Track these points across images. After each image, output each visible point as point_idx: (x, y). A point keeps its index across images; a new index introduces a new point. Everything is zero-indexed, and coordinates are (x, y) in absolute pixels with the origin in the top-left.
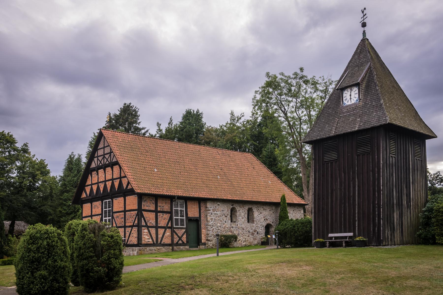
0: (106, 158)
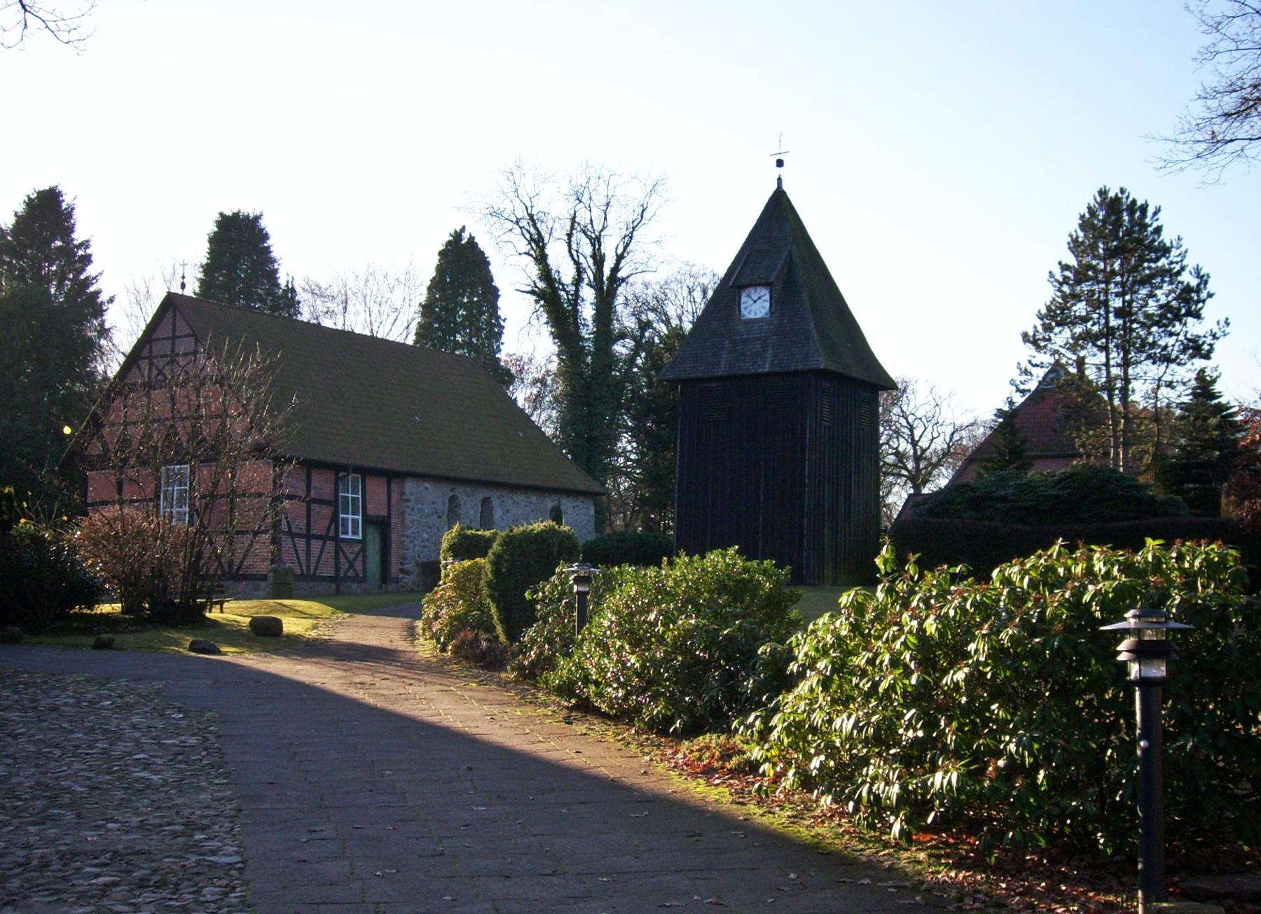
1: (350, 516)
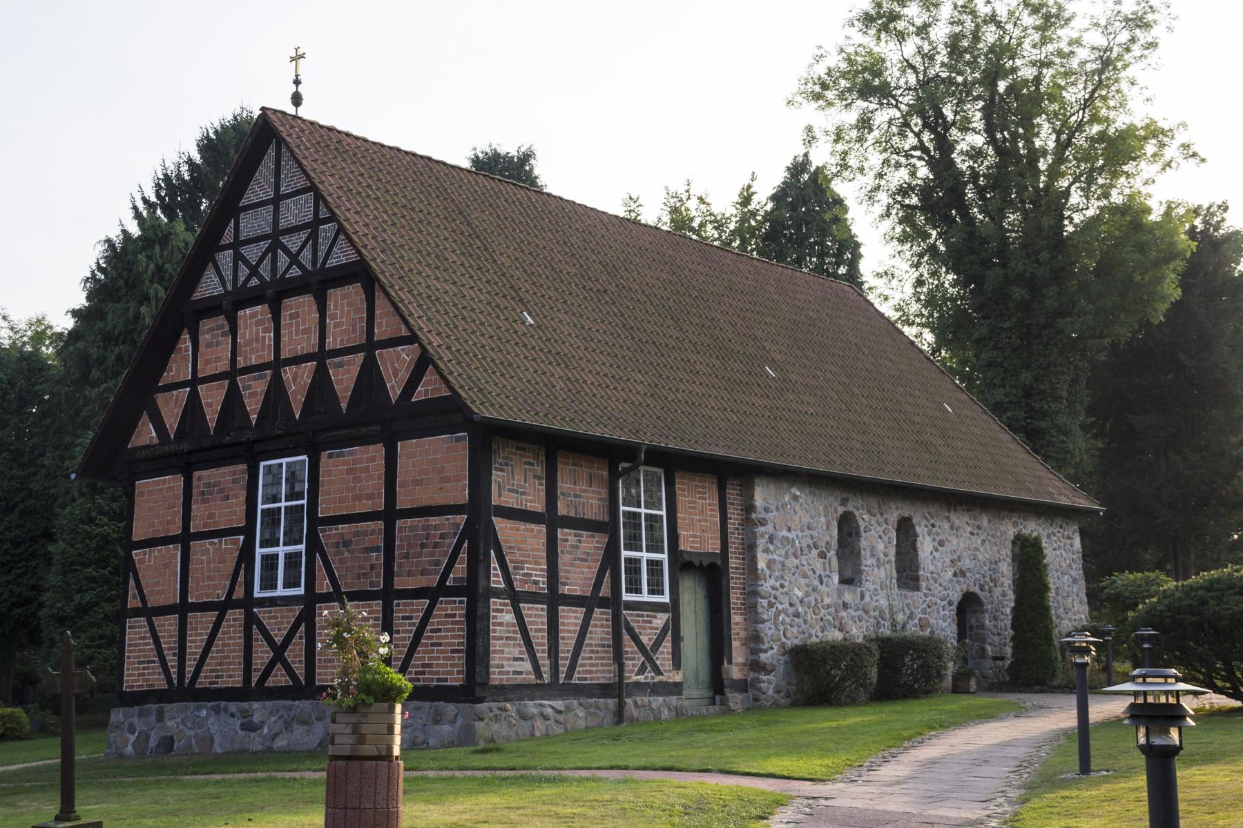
1: (644, 556)
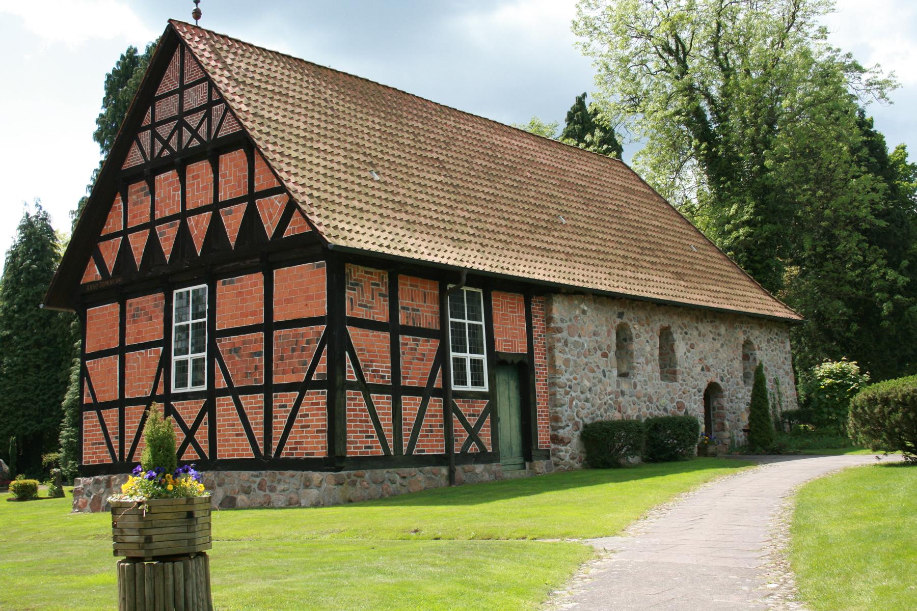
0: (189, 128)
1: (468, 356)
